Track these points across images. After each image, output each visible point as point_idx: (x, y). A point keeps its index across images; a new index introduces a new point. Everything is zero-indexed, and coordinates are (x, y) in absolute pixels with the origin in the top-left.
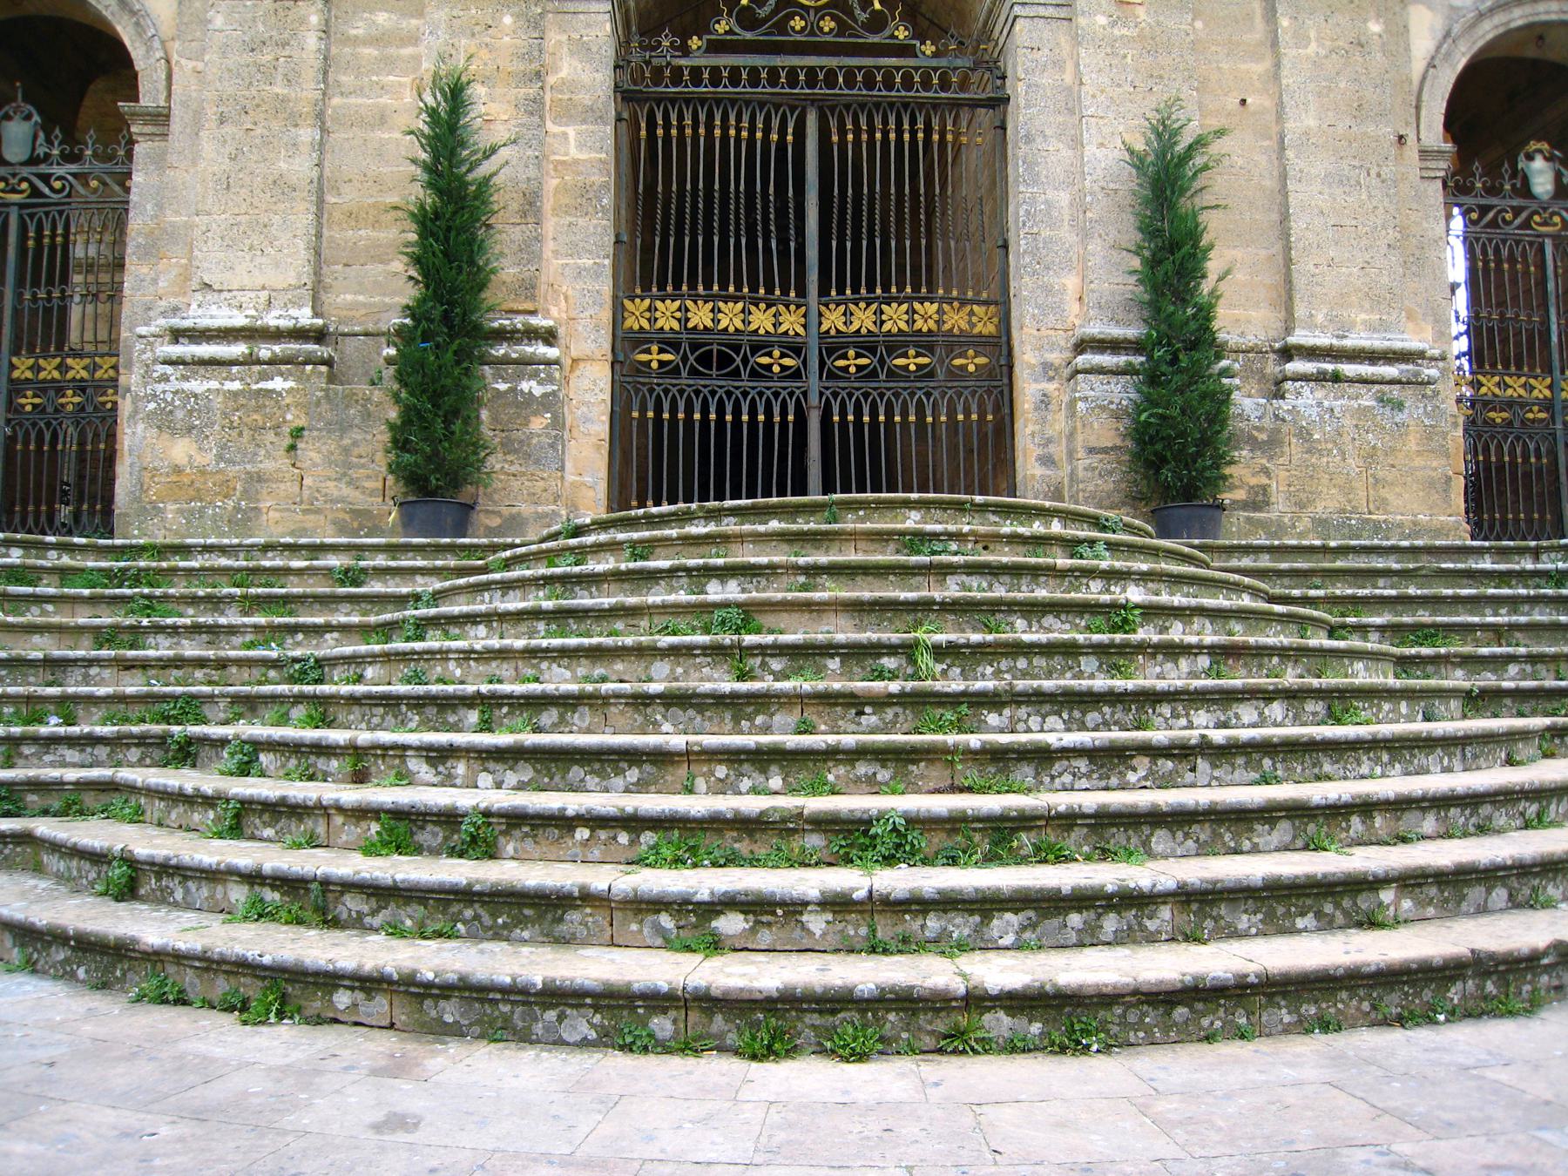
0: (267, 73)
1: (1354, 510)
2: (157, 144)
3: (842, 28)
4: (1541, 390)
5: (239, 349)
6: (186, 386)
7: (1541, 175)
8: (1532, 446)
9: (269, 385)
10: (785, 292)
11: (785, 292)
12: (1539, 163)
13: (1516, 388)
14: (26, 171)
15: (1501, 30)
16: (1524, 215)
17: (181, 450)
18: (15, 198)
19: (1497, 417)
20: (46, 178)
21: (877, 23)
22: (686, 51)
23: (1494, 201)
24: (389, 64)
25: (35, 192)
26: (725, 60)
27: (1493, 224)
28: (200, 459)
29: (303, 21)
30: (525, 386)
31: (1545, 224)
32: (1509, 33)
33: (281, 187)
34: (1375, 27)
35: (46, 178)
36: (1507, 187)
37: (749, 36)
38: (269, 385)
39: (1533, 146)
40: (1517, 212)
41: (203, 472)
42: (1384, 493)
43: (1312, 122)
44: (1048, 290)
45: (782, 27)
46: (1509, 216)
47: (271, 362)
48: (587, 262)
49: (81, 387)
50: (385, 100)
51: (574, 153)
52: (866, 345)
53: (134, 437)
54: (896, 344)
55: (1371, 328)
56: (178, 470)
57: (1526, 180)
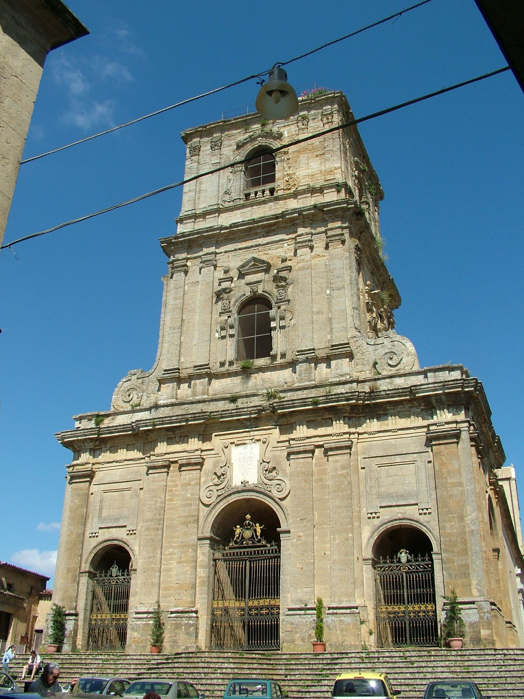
0: (151, 562)
1: (338, 642)
2: (135, 575)
3: (253, 543)
4: (402, 609)
5: (145, 615)
6: (137, 623)
9: (149, 622)
10: (242, 598)
11: (242, 598)
12: (403, 554)
16: (399, 567)
17: (135, 634)
18: (114, 583)
19: (392, 616)
20: (118, 579)
21: (259, 541)
22: (225, 550)
24: (171, 559)
25: (117, 582)
26: (232, 551)
27: (392, 570)
28: (138, 636)
29: (157, 553)
30: (190, 622)
33: (153, 584)
34: (350, 535)
35: (118, 579)
37: (236, 546)
38: (149, 622)
39: (402, 550)
40: (397, 566)
41: (139, 638)
42: (345, 638)
43: (336, 558)
44: (285, 597)
45: (242, 543)
47: (150, 618)
48: (203, 596)
49: (123, 620)
50: (171, 566)
51: (202, 575)
53: (129, 631)
55: (347, 601)
56: (135, 638)
57: (400, 559)
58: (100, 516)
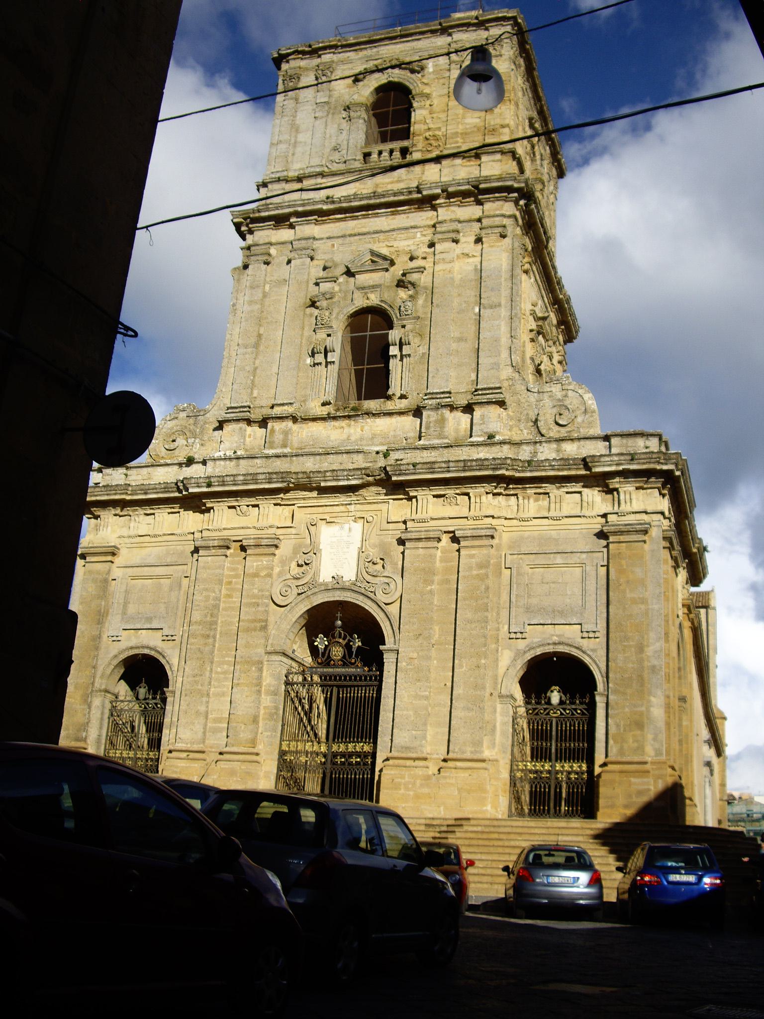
0: (196, 682)
4: (547, 767)
7: (555, 697)
8: (542, 785)
13: (538, 766)
14: (143, 702)
15: (533, 656)
16: (547, 711)
23: (538, 706)
27: (537, 714)
29: (206, 669)
31: (555, 713)
32: (536, 657)
33: (198, 713)
35: (148, 704)
36: (543, 702)
39: (553, 688)
46: (542, 711)
52: (343, 755)
54: (351, 755)
57: (549, 699)
58: (124, 613)
